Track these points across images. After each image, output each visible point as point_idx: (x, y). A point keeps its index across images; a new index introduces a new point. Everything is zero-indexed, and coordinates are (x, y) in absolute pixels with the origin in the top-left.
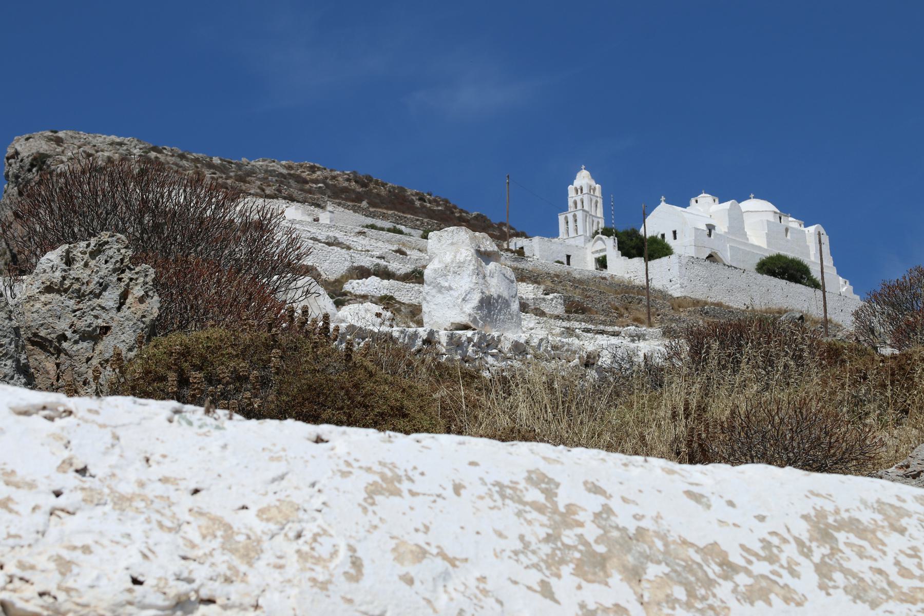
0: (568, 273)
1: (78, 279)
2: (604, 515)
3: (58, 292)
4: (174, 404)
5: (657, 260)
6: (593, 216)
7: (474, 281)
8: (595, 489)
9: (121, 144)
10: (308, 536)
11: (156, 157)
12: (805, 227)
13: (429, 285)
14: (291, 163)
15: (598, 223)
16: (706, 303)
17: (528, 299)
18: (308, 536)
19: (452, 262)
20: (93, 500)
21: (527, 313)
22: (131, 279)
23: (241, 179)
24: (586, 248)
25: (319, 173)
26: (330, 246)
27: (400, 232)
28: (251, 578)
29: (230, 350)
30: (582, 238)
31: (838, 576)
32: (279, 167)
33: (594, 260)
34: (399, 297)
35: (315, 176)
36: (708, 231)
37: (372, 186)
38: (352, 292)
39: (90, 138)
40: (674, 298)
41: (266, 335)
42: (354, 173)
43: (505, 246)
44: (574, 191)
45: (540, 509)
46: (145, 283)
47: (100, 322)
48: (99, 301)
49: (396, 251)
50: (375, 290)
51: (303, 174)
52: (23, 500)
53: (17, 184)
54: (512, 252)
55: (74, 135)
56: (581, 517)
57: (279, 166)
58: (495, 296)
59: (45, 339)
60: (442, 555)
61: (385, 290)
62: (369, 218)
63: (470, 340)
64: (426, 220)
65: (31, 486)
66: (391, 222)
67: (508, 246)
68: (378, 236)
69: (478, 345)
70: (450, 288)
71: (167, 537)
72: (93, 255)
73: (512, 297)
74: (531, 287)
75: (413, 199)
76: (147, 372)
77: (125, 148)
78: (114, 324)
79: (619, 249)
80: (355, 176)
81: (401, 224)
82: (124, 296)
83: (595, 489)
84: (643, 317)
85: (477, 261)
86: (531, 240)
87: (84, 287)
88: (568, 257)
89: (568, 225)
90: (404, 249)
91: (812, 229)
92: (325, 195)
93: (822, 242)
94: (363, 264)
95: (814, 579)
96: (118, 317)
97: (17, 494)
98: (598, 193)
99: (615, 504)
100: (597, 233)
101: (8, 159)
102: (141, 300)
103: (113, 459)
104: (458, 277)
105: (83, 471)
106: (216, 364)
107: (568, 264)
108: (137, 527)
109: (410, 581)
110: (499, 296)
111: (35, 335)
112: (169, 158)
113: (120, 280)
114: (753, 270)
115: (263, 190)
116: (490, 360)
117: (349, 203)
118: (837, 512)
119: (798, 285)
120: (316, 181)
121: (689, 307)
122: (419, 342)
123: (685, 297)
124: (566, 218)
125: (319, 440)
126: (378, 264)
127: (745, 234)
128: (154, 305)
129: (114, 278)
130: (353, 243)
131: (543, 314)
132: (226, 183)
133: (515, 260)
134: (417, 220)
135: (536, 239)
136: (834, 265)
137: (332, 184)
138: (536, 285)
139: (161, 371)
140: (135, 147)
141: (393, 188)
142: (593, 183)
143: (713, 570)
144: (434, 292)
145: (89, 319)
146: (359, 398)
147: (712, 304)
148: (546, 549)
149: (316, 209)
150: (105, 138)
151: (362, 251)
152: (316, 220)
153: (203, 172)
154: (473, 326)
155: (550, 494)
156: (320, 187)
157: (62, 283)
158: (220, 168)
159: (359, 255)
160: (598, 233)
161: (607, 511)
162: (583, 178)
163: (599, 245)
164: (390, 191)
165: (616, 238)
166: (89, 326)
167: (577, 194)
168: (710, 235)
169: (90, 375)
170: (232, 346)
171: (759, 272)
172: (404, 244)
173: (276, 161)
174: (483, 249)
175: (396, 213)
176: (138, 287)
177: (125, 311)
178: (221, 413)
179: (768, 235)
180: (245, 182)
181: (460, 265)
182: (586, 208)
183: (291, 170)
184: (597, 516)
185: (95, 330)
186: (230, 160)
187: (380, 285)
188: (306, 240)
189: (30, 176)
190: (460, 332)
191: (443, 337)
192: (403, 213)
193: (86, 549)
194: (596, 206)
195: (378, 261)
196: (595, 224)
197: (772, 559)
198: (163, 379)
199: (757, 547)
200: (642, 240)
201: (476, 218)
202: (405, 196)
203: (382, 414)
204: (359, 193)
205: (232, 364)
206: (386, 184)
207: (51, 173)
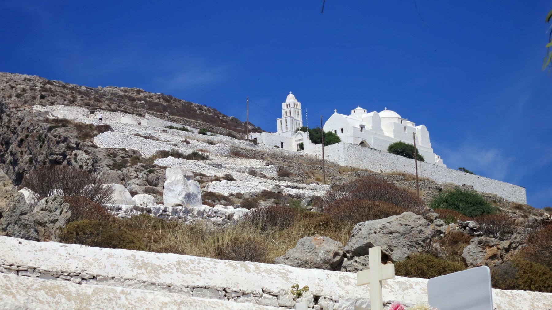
0: (281, 153)
1: (49, 207)
2: (143, 261)
3: (45, 210)
4: (81, 245)
5: (332, 145)
6: (296, 120)
7: (183, 187)
8: (142, 257)
9: (30, 80)
10: (99, 263)
11: (50, 88)
12: (416, 126)
13: (166, 189)
14: (126, 88)
15: (299, 124)
16: (358, 170)
17: (257, 168)
18: (99, 263)
19: (175, 180)
20: (71, 258)
21: (255, 176)
22: (63, 207)
23: (97, 100)
24: (292, 139)
25: (142, 94)
26: (146, 139)
27: (187, 130)
28: (91, 267)
29: (89, 226)
30: (290, 133)
31: (180, 270)
32: (119, 91)
33: (296, 145)
35: (140, 96)
36: (361, 129)
37: (172, 101)
38: (159, 165)
39: (13, 76)
40: (341, 167)
41: (99, 222)
42: (162, 94)
44: (285, 106)
45: (133, 260)
46: (67, 208)
47: (55, 218)
48: (55, 213)
49: (184, 141)
50: (171, 164)
51: (133, 95)
52: (63, 258)
54: (250, 141)
55: (3, 75)
56: (139, 261)
57: (119, 91)
58: (191, 193)
59: (41, 223)
60: (117, 265)
61: (177, 164)
62: (169, 122)
63: (181, 210)
64: (201, 122)
65: (63, 256)
66: (181, 124)
67: (248, 137)
68: (174, 133)
69: (184, 212)
70: (174, 190)
71: (80, 262)
72: (53, 200)
73: (198, 193)
74: (259, 161)
75: (196, 109)
76: (68, 232)
77: (32, 82)
78: (59, 219)
79: (311, 139)
80: (163, 96)
81: (187, 125)
82: (62, 211)
83: (142, 257)
84: (322, 178)
85: (184, 180)
86: (261, 134)
87: (51, 209)
88: (282, 143)
89: (287, 124)
90: (188, 140)
91: (420, 127)
93: (415, 138)
94: (165, 149)
95: (176, 270)
96: (60, 217)
97: (62, 257)
98: (299, 106)
99: (145, 259)
100: (298, 130)
102: (66, 212)
103: (73, 252)
104: (177, 186)
105: (69, 254)
106: (86, 230)
107: (282, 147)
108: (77, 261)
109: (113, 269)
110: (193, 193)
111: (39, 222)
112: (57, 88)
113: (60, 207)
114: (386, 151)
115: (110, 106)
116: (189, 217)
117: (158, 113)
118: (182, 260)
119: (410, 159)
120: (140, 99)
121: (349, 172)
122: (161, 211)
123: (347, 166)
124: (281, 121)
125: (101, 250)
126: (173, 150)
127: (382, 130)
128: (69, 214)
129: (59, 207)
130: (160, 137)
131: (265, 177)
132: (89, 102)
133: (251, 145)
134: (197, 122)
135: (264, 134)
136: (432, 147)
137: (149, 101)
138: (261, 160)
139: (72, 231)
140: (38, 81)
141: (185, 103)
142: (296, 101)
143: (159, 269)
144: (168, 192)
145: (52, 218)
146: (122, 238)
148: (133, 265)
149: (139, 117)
150: (21, 76)
151: (165, 141)
152: (140, 124)
153: (76, 97)
154: (182, 205)
155: (135, 258)
156: (142, 103)
157: (45, 208)
158: (86, 93)
159: (163, 144)
160: (299, 130)
161: (143, 260)
162: (291, 99)
163: (299, 137)
164: (182, 105)
165: (309, 133)
166: (53, 219)
167: (287, 107)
168: (362, 131)
169: (53, 232)
170: (90, 225)
171: (389, 152)
172: (189, 137)
173: (117, 87)
174: (187, 175)
175: (185, 118)
176: (65, 209)
177: (62, 215)
178: (87, 246)
179: (395, 131)
180: (100, 101)
181: (178, 182)
182: (292, 115)
183: (126, 93)
184: (141, 261)
185: (54, 220)
186: (92, 88)
187: (174, 161)
188: (133, 136)
190: (177, 207)
191: (170, 209)
192: (189, 118)
193: (71, 264)
194: (298, 114)
196: (298, 124)
197: (169, 267)
198: (72, 233)
199: (167, 265)
201: (232, 119)
202: (191, 107)
203: (128, 243)
204: (164, 106)
205: (90, 230)
206: (181, 101)
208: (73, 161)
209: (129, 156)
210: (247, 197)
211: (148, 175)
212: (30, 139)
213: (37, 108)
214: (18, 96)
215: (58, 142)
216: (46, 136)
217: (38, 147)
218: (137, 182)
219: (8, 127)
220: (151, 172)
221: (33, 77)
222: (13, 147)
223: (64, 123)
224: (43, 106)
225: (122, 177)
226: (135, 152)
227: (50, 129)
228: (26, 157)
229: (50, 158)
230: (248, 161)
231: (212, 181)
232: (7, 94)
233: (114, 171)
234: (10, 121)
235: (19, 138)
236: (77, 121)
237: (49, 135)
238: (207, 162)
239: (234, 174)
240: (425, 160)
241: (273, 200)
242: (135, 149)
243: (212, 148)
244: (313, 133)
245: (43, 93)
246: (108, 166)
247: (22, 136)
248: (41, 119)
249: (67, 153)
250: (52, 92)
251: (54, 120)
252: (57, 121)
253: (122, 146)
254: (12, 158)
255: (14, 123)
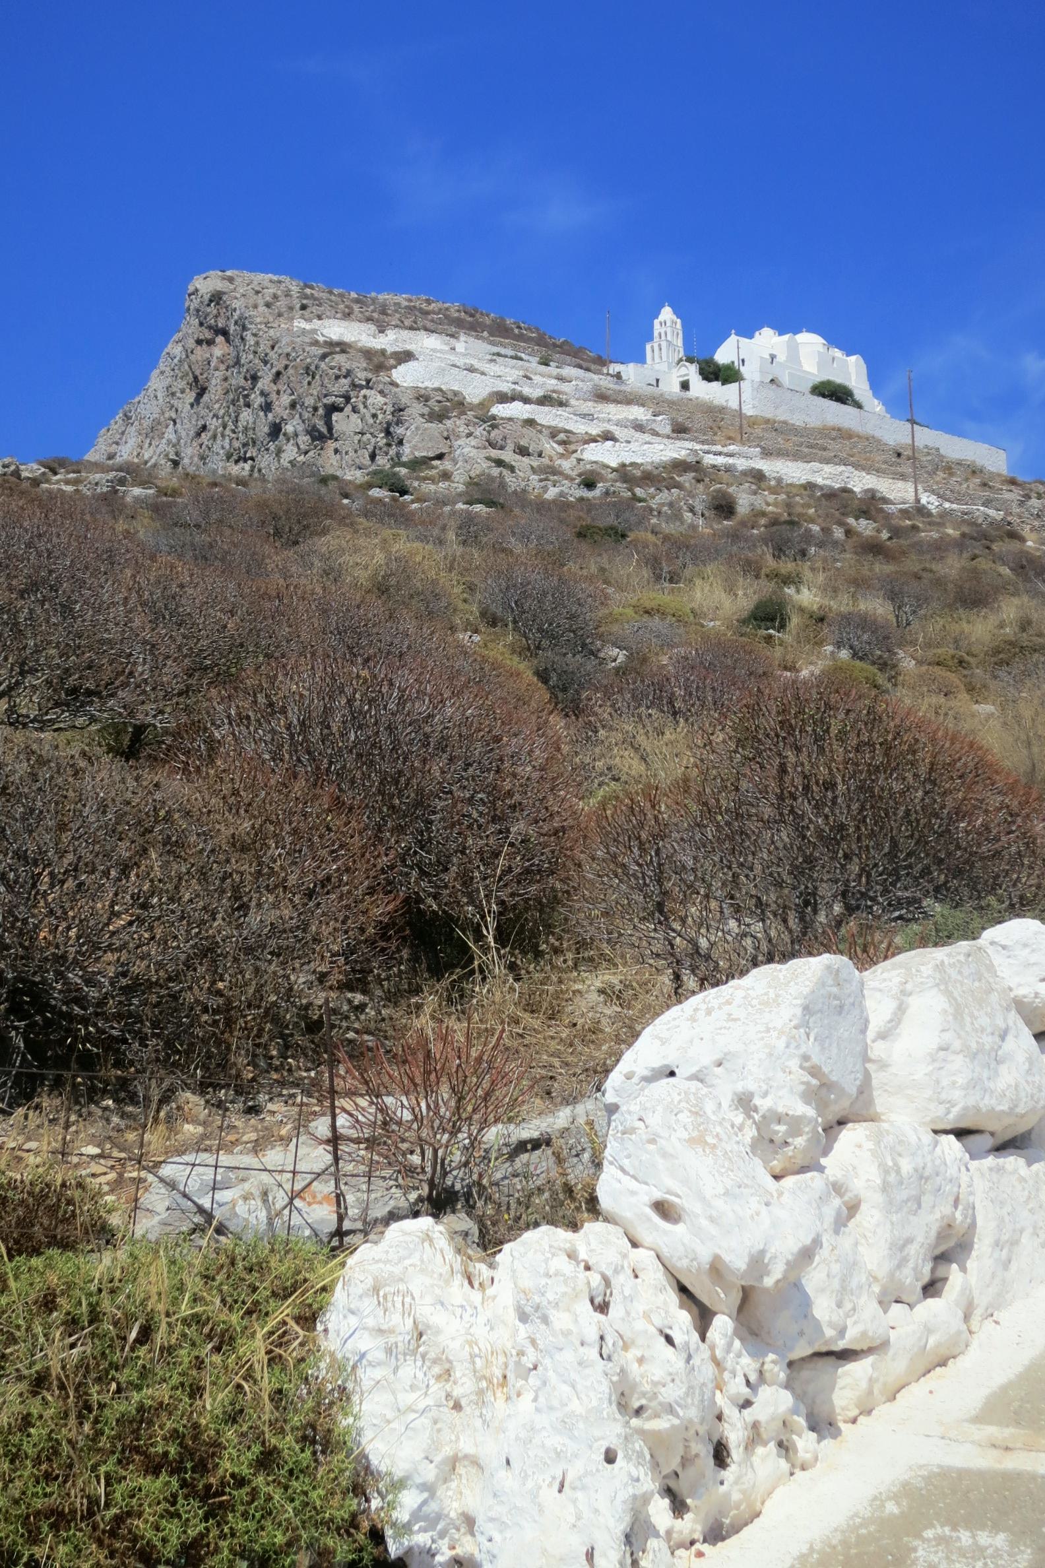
9: (280, 282)
27: (521, 359)
34: (541, 420)
37: (478, 316)
43: (605, 371)
53: (198, 316)
74: (642, 409)
88: (658, 381)
91: (853, 358)
92: (406, 307)
98: (679, 326)
100: (681, 360)
101: (190, 295)
133: (617, 383)
135: (631, 365)
142: (674, 317)
147: (780, 422)
162: (667, 314)
163: (683, 371)
179: (819, 363)
182: (669, 338)
189: (209, 310)
195: (513, 386)
200: (716, 365)
207: (227, 308)
208: (361, 406)
209: (448, 400)
210: (649, 468)
211: (489, 432)
212: (291, 371)
213: (300, 324)
214: (268, 305)
215: (337, 377)
216: (317, 367)
217: (305, 383)
218: (473, 443)
219: (255, 352)
220: (494, 427)
221: (282, 278)
222: (265, 383)
223: (342, 347)
224: (309, 320)
225: (445, 434)
226: (456, 393)
227: (324, 357)
228: (286, 399)
229: (325, 401)
230: (620, 407)
231: (587, 442)
232: (251, 302)
233: (434, 425)
234: (257, 343)
235: (274, 370)
236: (360, 345)
237: (323, 365)
238: (568, 409)
239: (617, 431)
240: (866, 408)
241: (693, 474)
242: (456, 388)
243: (565, 387)
244: (704, 365)
245: (305, 302)
246: (423, 415)
247: (279, 366)
248: (307, 340)
249: (352, 394)
250: (316, 299)
251: (325, 342)
252: (331, 344)
253: (436, 385)
254: (263, 400)
255: (264, 347)
